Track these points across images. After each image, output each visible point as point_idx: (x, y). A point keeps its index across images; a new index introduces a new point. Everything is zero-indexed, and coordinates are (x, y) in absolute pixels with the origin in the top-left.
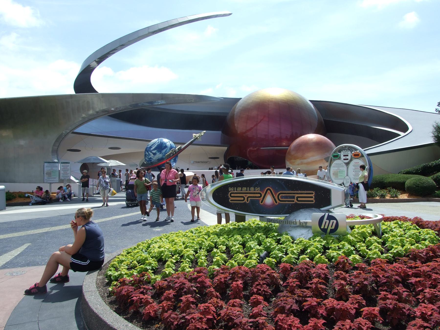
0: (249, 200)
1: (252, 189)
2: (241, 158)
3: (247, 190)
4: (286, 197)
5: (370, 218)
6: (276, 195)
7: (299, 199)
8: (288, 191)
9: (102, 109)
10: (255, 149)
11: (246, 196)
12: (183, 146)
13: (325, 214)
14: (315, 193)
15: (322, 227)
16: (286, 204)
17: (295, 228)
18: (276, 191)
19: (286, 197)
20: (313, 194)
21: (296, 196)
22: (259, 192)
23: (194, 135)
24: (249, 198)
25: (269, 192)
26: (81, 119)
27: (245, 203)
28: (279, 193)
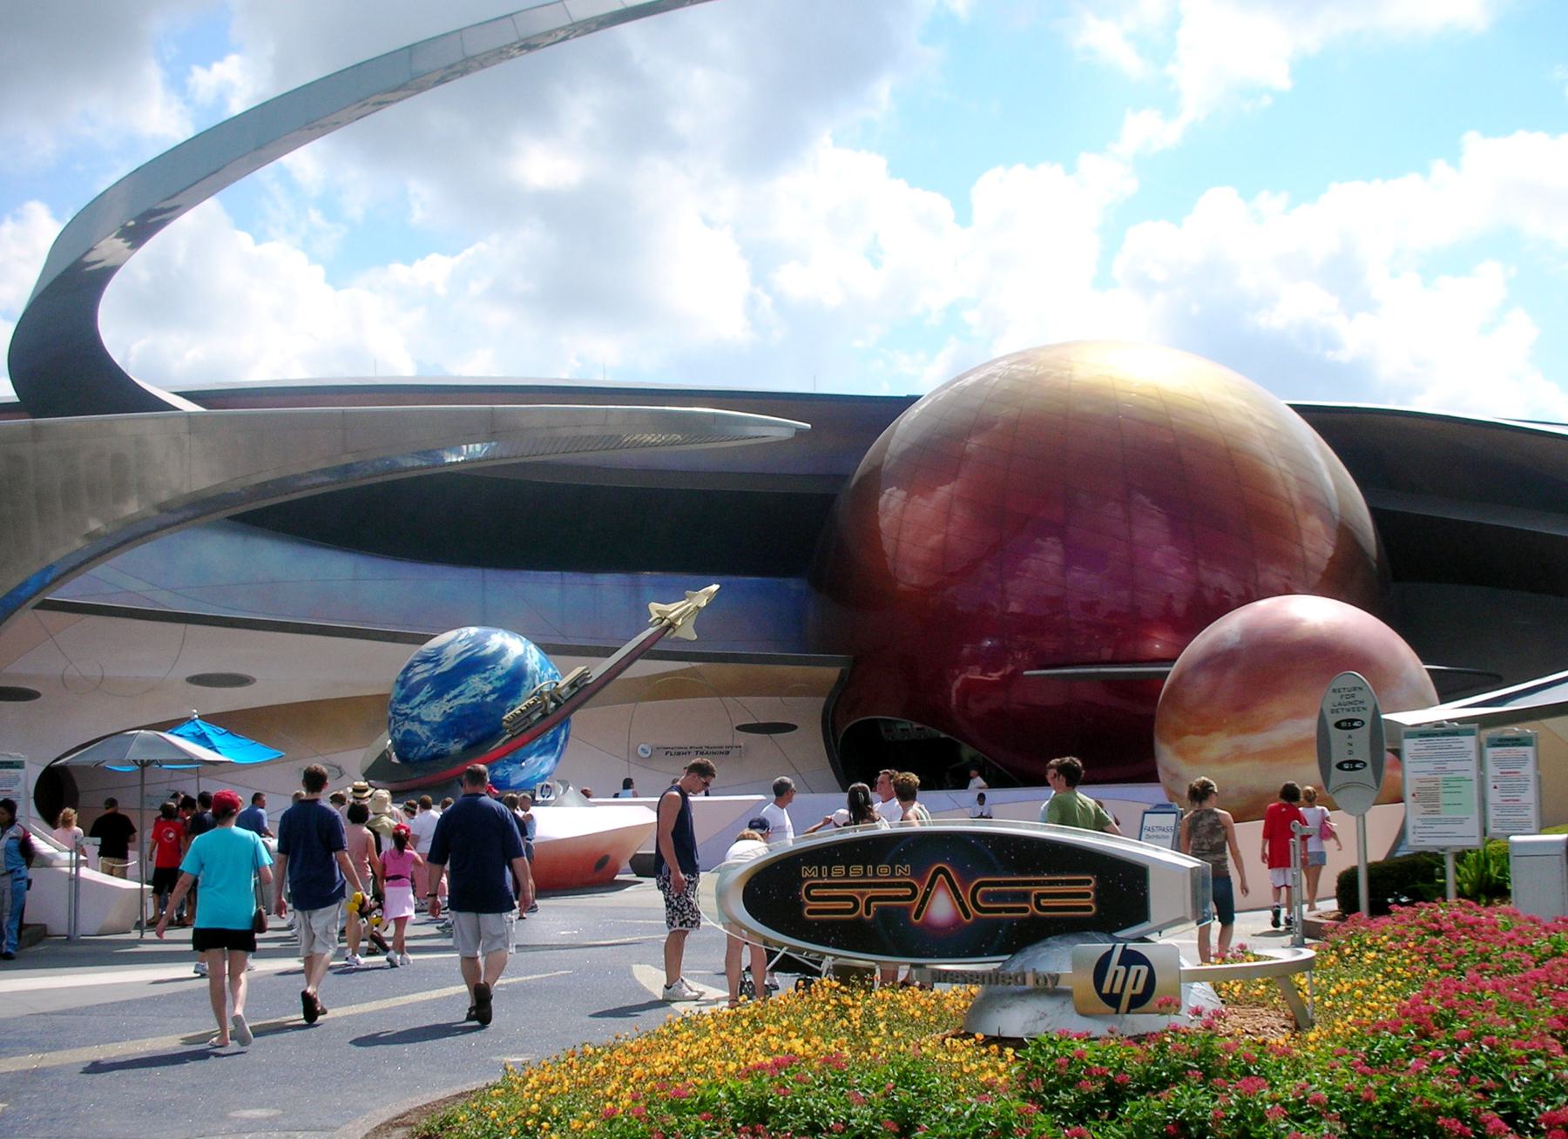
0: (873, 910)
1: (884, 869)
2: (916, 726)
3: (865, 875)
4: (999, 897)
5: (1271, 958)
6: (965, 891)
7: (1043, 902)
8: (1006, 876)
9: (186, 490)
10: (995, 676)
11: (862, 895)
12: (601, 667)
13: (1114, 947)
14: (1097, 880)
15: (1106, 989)
16: (1000, 922)
17: (1023, 998)
18: (966, 877)
19: (999, 897)
20: (1088, 885)
21: (1035, 892)
22: (908, 880)
23: (655, 607)
24: (873, 904)
25: (941, 878)
26: (79, 543)
27: (859, 920)
28: (976, 882)
